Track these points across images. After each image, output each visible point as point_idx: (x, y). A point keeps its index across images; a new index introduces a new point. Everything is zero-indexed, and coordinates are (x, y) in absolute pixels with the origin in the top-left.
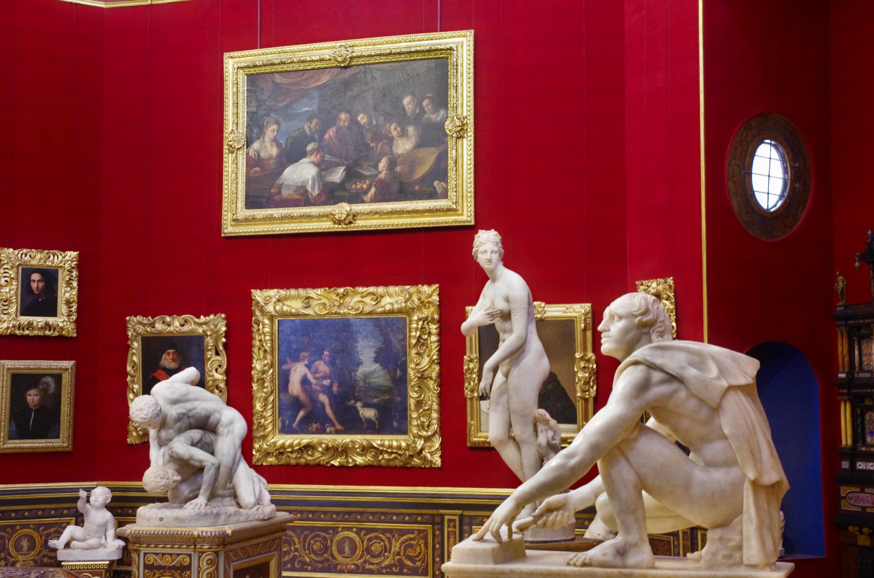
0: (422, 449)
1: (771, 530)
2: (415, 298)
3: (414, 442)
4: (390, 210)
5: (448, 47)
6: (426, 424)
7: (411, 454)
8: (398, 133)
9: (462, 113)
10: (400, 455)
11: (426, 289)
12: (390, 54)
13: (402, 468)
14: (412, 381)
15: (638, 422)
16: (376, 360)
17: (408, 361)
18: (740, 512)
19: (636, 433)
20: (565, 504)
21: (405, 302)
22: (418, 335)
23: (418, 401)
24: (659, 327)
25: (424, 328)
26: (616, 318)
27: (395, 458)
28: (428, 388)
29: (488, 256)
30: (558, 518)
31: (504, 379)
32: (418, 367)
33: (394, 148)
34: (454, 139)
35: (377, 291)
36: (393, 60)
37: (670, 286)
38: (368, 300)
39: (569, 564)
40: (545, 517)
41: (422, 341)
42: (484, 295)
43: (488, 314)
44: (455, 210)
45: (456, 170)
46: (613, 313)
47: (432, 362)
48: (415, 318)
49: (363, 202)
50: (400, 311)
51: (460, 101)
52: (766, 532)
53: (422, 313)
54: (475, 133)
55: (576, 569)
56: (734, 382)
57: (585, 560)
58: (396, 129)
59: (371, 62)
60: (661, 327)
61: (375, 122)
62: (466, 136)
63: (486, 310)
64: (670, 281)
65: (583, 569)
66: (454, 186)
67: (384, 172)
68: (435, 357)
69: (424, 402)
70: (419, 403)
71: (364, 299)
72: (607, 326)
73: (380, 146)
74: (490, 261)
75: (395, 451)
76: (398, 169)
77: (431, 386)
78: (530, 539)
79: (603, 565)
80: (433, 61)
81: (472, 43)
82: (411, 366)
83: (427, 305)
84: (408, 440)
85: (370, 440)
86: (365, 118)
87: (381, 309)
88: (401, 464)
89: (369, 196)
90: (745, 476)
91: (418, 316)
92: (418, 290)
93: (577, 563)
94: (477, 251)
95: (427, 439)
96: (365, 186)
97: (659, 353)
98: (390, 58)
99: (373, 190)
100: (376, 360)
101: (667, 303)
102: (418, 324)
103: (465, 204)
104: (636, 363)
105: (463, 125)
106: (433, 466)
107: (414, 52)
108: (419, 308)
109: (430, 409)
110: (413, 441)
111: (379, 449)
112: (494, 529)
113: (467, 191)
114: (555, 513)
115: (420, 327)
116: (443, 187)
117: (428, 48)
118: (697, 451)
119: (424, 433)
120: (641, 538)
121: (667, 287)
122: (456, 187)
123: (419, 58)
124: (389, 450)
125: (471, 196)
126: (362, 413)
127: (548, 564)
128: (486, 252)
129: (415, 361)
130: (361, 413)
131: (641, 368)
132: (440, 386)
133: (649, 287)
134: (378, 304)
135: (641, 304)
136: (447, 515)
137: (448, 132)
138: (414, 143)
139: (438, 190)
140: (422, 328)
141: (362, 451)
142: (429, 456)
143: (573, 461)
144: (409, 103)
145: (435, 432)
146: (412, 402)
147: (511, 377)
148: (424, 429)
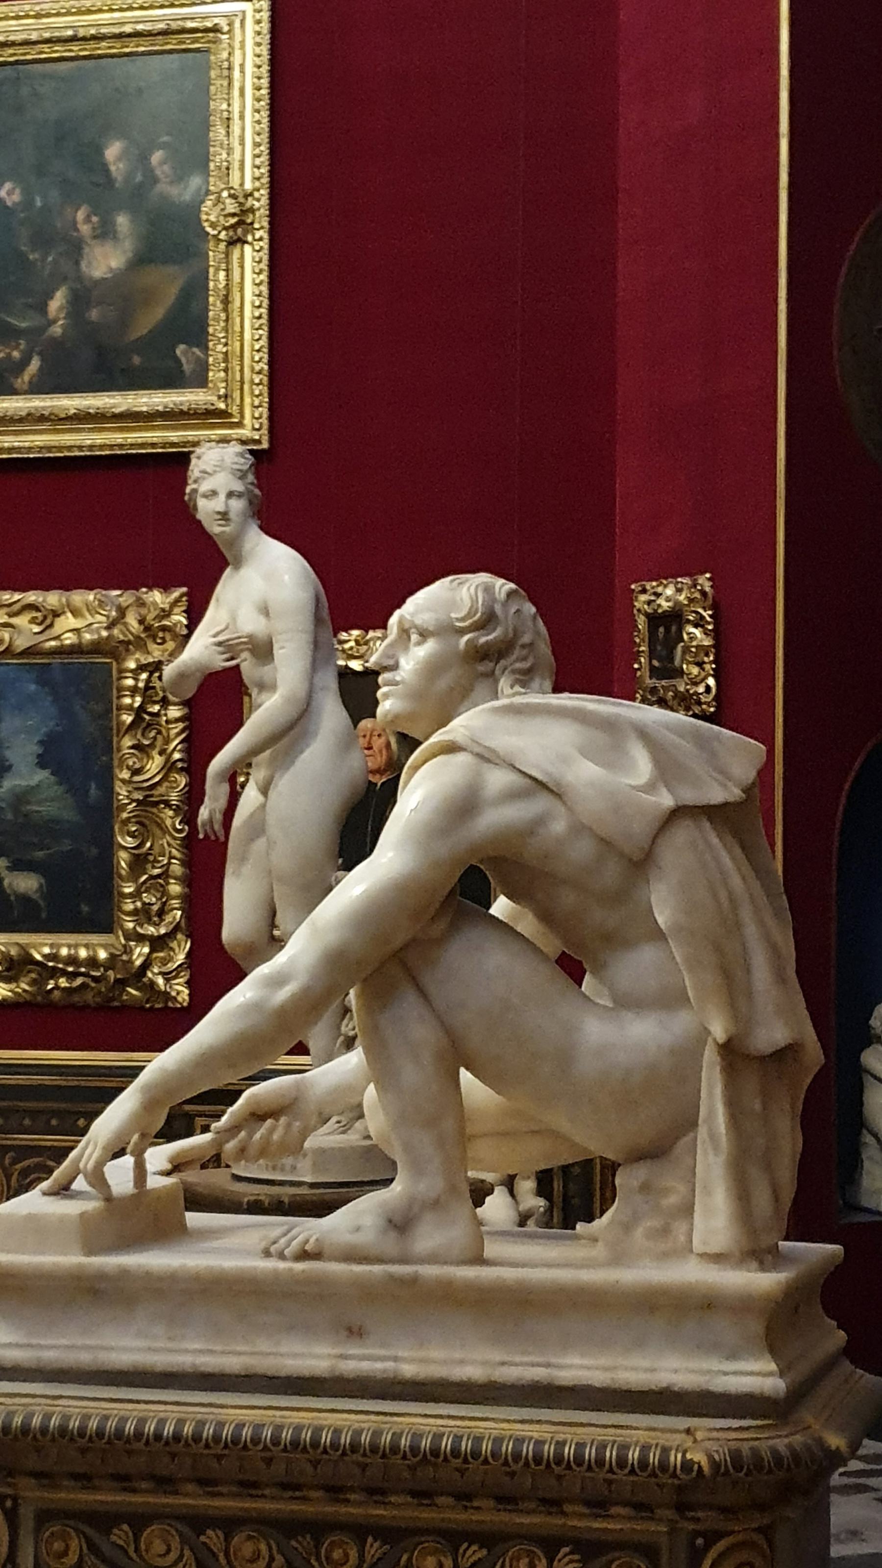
0: (147, 965)
1: (768, 1167)
2: (132, 620)
3: (128, 951)
4: (73, 411)
5: (209, 24)
6: (155, 908)
7: (119, 976)
8: (94, 229)
9: (242, 184)
10: (96, 979)
11: (157, 597)
12: (74, 39)
13: (99, 1008)
14: (124, 810)
15: (452, 892)
16: (42, 762)
17: (116, 763)
18: (692, 1124)
19: (442, 925)
20: (296, 1099)
21: (108, 628)
22: (137, 705)
23: (137, 856)
24: (517, 660)
25: (154, 688)
26: (414, 637)
27: (84, 986)
28: (159, 825)
29: (218, 504)
30: (275, 1137)
31: (261, 798)
32: (137, 778)
33: (83, 265)
34: (222, 246)
35: (44, 601)
36: (82, 53)
37: (704, 593)
38: (22, 621)
39: (267, 1253)
40: (243, 1134)
41: (147, 717)
42: (217, 600)
43: (220, 644)
44: (224, 414)
45: (227, 320)
46: (407, 626)
47: (169, 767)
48: (132, 665)
49: (14, 392)
50: (96, 648)
51: (237, 156)
52: (755, 1173)
53: (148, 653)
54: (272, 233)
55: (282, 1265)
56: (690, 796)
57: (307, 1241)
58: (88, 220)
59: (29, 57)
60: (524, 659)
61: (39, 203)
62: (250, 238)
63: (215, 636)
64: (704, 581)
65: (300, 1266)
66: (221, 356)
67: (60, 322)
68: (177, 756)
69: (151, 858)
70: (139, 862)
71: (14, 621)
72: (392, 657)
73: (50, 259)
74: (224, 516)
75: (83, 970)
76: (94, 314)
77: (168, 822)
78: (308, 1179)
79: (352, 1256)
80: (175, 56)
81: (265, 15)
82: (121, 776)
83: (161, 634)
84: (112, 945)
85: (27, 944)
86: (18, 191)
87: (53, 643)
88: (98, 1000)
89: (26, 378)
90: (708, 1032)
91: (137, 660)
92: (139, 599)
93: (286, 1252)
94: (195, 491)
95: (158, 943)
96: (16, 354)
97: (509, 722)
98: (75, 49)
99: (35, 364)
100: (42, 762)
101: (697, 632)
102: (136, 680)
103: (247, 400)
104: (451, 748)
105: (244, 212)
106: (170, 1004)
107: (129, 35)
108: (139, 644)
109: (165, 875)
110: (125, 946)
111: (46, 965)
112: (91, 1165)
113: (252, 370)
114: (269, 1122)
115: (141, 685)
116: (198, 358)
117: (162, 26)
118: (599, 969)
119: (151, 930)
120: (452, 1189)
121: (697, 595)
122: (226, 360)
123: (142, 49)
124: (70, 969)
125: (260, 383)
126: (10, 884)
127: (230, 1252)
128: (214, 493)
129: (131, 763)
130: (6, 883)
131: (461, 759)
132: (187, 823)
133: (658, 595)
134: (47, 632)
135: (474, 601)
136: (200, 1116)
137: (209, 229)
138: (130, 255)
139: (186, 367)
140: (147, 688)
141: (8, 969)
142: (160, 981)
143: (284, 994)
144: (119, 159)
145: (177, 928)
146: (123, 859)
147: (272, 794)
148: (149, 921)
